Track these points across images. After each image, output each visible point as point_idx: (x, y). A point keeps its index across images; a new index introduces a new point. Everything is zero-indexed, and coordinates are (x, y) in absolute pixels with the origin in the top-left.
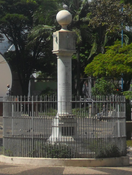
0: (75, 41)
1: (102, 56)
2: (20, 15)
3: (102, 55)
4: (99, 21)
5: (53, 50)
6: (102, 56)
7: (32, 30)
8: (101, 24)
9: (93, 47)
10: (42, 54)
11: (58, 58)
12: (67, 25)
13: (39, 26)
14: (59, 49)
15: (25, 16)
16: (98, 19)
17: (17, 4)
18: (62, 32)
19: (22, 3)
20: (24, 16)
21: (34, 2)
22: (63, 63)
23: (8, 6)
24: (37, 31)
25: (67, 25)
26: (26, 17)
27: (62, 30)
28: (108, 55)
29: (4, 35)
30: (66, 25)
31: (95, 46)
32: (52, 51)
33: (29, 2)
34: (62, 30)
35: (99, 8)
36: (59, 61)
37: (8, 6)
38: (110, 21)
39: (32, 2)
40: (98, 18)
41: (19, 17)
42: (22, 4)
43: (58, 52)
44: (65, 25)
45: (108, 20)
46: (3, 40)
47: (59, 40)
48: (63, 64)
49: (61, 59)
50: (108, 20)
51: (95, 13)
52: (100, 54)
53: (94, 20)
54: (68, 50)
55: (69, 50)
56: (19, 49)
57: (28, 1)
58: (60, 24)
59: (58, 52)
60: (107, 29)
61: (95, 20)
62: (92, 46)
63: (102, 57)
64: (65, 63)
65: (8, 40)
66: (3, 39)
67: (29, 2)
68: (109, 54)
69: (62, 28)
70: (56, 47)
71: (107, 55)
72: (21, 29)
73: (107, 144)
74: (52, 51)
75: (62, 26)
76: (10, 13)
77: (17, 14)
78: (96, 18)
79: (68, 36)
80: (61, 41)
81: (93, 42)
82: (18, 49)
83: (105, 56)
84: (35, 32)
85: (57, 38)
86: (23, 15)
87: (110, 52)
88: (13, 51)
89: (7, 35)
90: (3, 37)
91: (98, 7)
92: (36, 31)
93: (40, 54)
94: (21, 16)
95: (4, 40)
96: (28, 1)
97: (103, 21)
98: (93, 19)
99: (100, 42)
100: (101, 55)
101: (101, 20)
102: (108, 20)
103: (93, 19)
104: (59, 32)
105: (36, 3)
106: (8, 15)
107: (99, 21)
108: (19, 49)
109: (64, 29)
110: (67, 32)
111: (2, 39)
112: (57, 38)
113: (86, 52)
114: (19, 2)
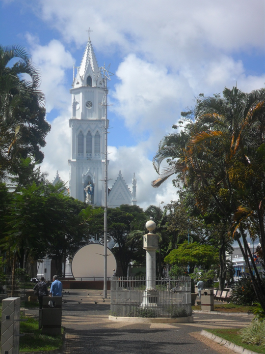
4: (173, 228)
27: (149, 233)
29: (111, 237)
34: (149, 233)
36: (148, 254)
70: (145, 245)
72: (122, 233)
97: (176, 228)
106: (114, 223)
107: (173, 228)
113: (165, 248)
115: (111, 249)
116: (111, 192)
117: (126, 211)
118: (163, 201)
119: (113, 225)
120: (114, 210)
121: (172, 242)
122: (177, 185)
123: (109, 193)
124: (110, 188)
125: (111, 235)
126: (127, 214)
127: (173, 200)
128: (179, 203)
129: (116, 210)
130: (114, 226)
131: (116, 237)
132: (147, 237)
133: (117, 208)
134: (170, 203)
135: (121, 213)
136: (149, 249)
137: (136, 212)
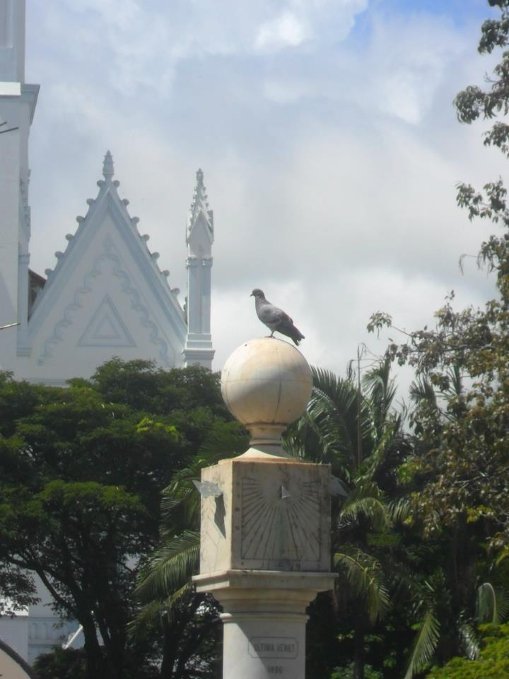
0: (329, 519)
1: (463, 668)
2: (106, 487)
3: (465, 662)
4: (454, 501)
5: (197, 573)
6: (463, 668)
7: (157, 554)
8: (463, 516)
9: (423, 637)
10: (203, 663)
11: (230, 620)
12: (284, 424)
13: (189, 535)
14: (233, 568)
15: (128, 495)
16: (451, 491)
17: (92, 438)
18: (252, 466)
19: (117, 432)
20: (127, 491)
21: (170, 432)
22: (257, 648)
23: (56, 445)
24: (180, 558)
25: (285, 428)
26: (136, 498)
27: (252, 454)
28: (491, 665)
29: (33, 577)
30: (278, 424)
31: (429, 630)
32: (195, 578)
33: (146, 429)
34: (252, 454)
35: (456, 437)
36: (233, 636)
37: (56, 445)
38: (504, 500)
39: (162, 429)
40: (448, 486)
41: (102, 496)
42: (116, 435)
43: (226, 584)
44: (273, 423)
45: (497, 494)
46: (34, 603)
47: (235, 509)
48: (255, 654)
49: (242, 626)
50: (499, 497)
51: (434, 465)
52: (456, 660)
53: (433, 493)
54: (288, 574)
55: (291, 570)
56: (101, 641)
57: (143, 427)
58: (244, 417)
59: (226, 584)
60: (489, 541)
61: (437, 493)
62: (416, 634)
63: (465, 673)
64: (269, 648)
65: (51, 599)
66: (34, 596)
67: (146, 429)
68: (495, 658)
69: (255, 446)
70: (215, 554)
71: (486, 662)
72: (113, 553)
73: (263, 505)
74: (195, 578)
75: (255, 431)
76: (62, 479)
77: (95, 485)
78: (443, 485)
79: (287, 488)
80: (247, 519)
81: (422, 610)
82: (98, 643)
83: (478, 668)
84: (169, 562)
85: (220, 500)
86: (123, 487)
87: (502, 651)
88: (83, 645)
89: (51, 579)
90: (32, 590)
91: (452, 436)
92: (175, 559)
93: (194, 666)
94: (113, 493)
95: (37, 600)
96: (145, 426)
97: (476, 501)
98: (428, 492)
99: (457, 611)
100: (460, 665)
101: (463, 494)
102: (499, 497)
103: (428, 492)
104: (236, 465)
105: (177, 435)
106: (54, 484)
107: (454, 501)
108: (101, 641)
109: (261, 447)
110: (281, 467)
111: (30, 596)
112: (220, 500)
113: (389, 663)
114: (102, 429)
115: (30, 658)
116: (45, 296)
117: (138, 405)
118: (385, 310)
119: (45, 495)
120: (54, 395)
121: (441, 614)
122: (486, 201)
123: (33, 297)
124: (42, 263)
125: (31, 564)
126: (144, 424)
127: (458, 308)
128: (495, 328)
129: (67, 397)
130: (50, 506)
131: (72, 588)
132: (227, 489)
133: (77, 383)
134: (434, 327)
135: (99, 418)
136: (247, 596)
137: (202, 414)
